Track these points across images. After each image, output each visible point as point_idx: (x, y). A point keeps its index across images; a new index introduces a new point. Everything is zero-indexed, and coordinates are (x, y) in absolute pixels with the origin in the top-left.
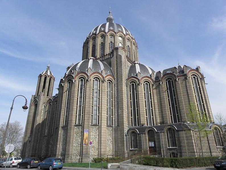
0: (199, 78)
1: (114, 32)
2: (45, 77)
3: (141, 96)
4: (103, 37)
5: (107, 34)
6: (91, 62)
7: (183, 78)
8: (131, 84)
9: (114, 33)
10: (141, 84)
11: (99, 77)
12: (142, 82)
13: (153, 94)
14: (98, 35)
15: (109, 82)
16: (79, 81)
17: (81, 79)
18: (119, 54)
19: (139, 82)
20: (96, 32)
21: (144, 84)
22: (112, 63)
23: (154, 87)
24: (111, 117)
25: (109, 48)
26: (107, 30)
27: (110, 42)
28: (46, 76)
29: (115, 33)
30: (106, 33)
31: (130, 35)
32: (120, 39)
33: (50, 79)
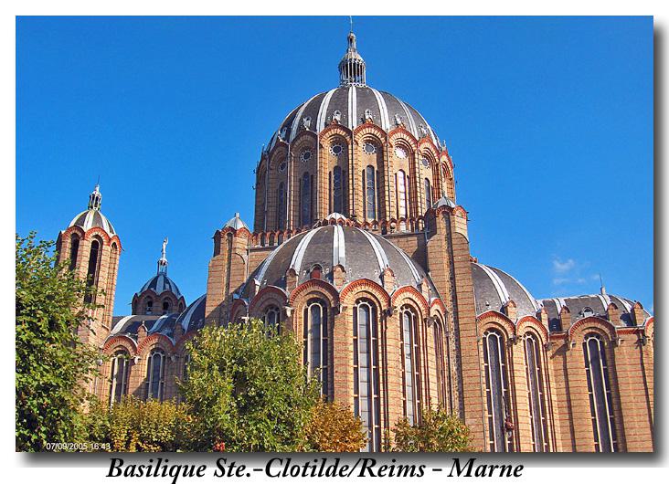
0: (547, 328)
1: (380, 129)
2: (94, 242)
3: (341, 347)
4: (341, 146)
5: (391, 141)
6: (339, 235)
7: (635, 337)
8: (309, 308)
9: (379, 135)
10: (345, 308)
11: (415, 306)
12: (348, 301)
13: (547, 375)
14: (321, 137)
15: (406, 312)
16: (306, 310)
18: (458, 230)
19: (515, 334)
20: (314, 127)
22: (430, 256)
23: (550, 354)
24: (542, 418)
25: (364, 188)
26: (353, 123)
27: (365, 168)
28: (97, 236)
29: (416, 142)
30: (349, 132)
31: (432, 143)
32: (400, 153)
33: (95, 245)
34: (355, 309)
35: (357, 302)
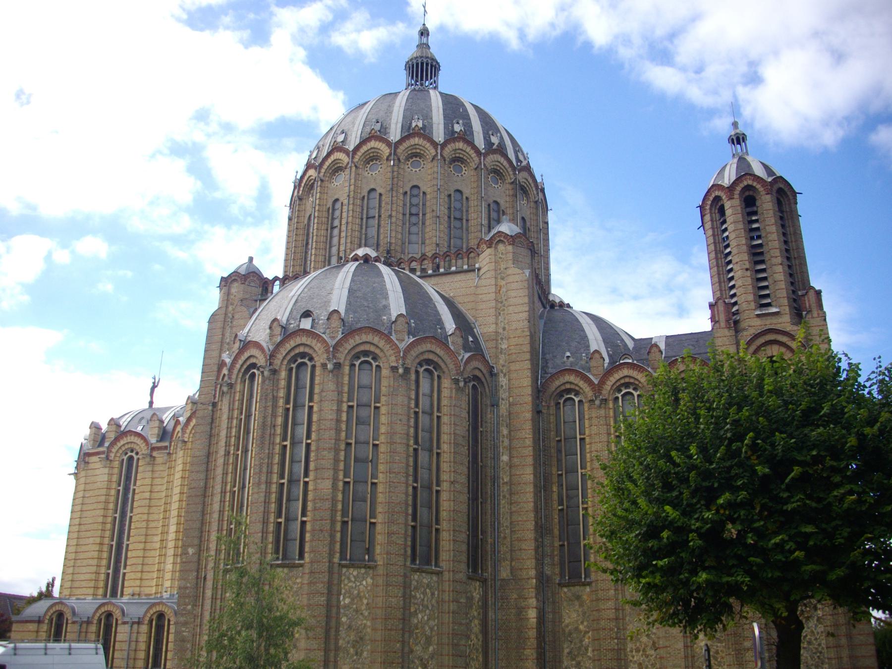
15: (426, 370)
17: (300, 361)
21: (417, 372)
34: (417, 372)
35: (420, 364)
